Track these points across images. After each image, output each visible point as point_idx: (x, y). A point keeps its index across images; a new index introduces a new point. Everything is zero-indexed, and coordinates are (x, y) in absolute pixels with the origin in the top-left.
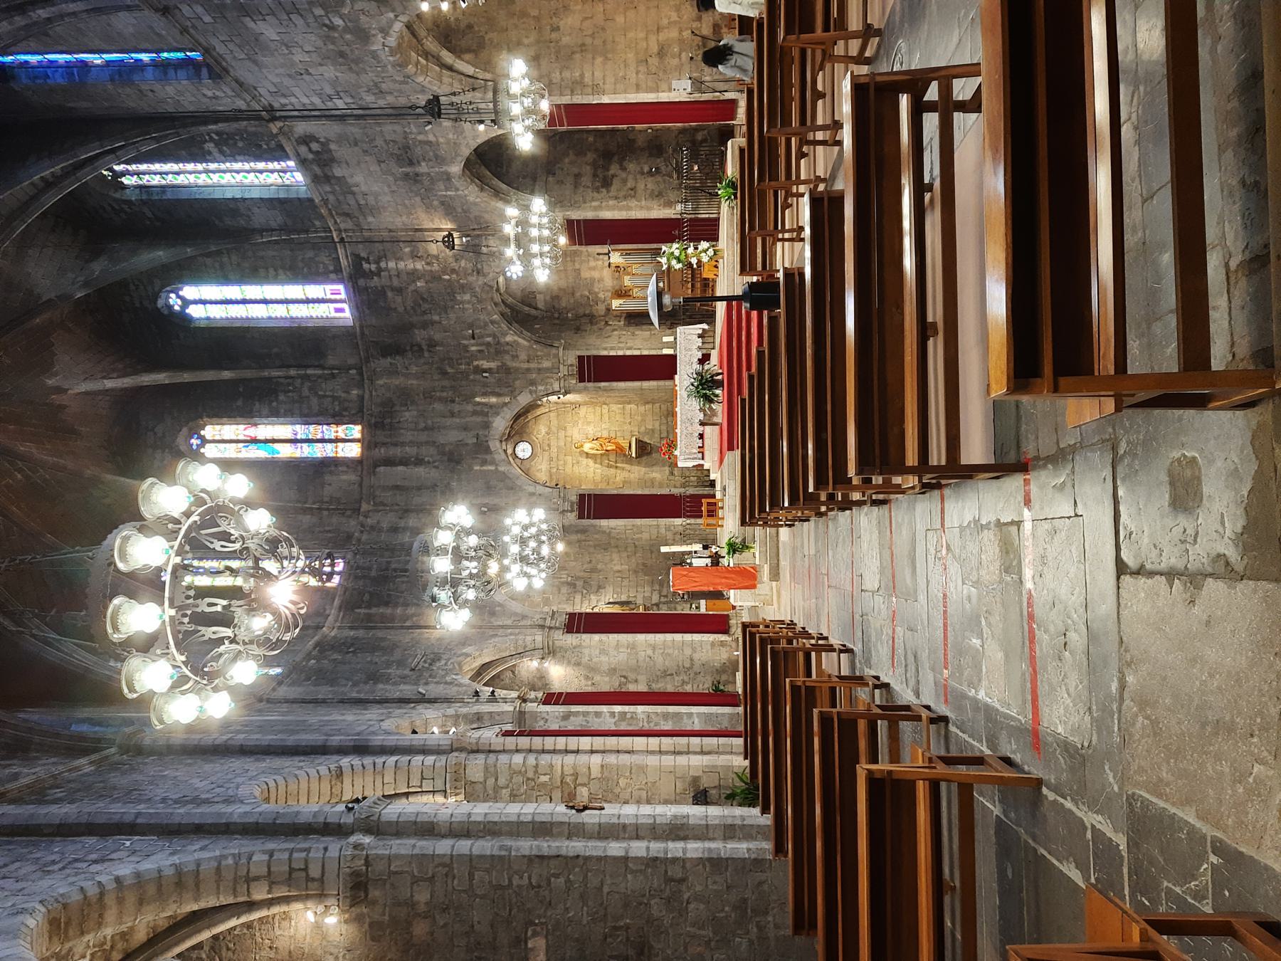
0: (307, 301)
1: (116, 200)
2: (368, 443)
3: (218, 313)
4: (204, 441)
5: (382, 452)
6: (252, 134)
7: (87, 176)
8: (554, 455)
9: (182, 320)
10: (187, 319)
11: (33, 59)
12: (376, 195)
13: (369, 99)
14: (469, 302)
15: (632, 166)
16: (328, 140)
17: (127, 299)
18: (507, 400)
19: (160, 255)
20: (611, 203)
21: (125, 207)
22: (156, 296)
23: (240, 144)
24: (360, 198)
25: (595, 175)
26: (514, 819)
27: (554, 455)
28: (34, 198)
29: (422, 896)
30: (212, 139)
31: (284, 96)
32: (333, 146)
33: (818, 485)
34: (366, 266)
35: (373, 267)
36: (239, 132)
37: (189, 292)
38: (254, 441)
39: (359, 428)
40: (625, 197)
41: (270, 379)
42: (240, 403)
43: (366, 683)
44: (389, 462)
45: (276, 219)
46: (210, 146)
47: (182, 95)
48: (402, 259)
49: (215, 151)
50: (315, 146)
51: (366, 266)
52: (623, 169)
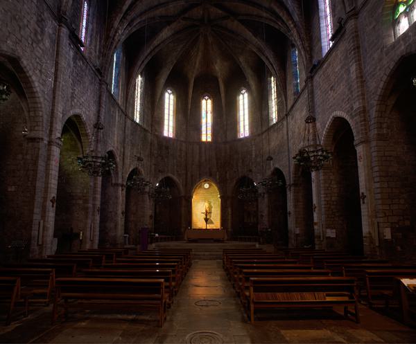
0: (244, 126)
3: (241, 102)
4: (206, 100)
6: (284, 113)
9: (238, 93)
10: (239, 95)
13: (292, 141)
19: (253, 87)
26: (50, 182)
29: (28, 157)
33: (255, 282)
37: (246, 95)
38: (207, 113)
39: (209, 139)
47: (290, 92)
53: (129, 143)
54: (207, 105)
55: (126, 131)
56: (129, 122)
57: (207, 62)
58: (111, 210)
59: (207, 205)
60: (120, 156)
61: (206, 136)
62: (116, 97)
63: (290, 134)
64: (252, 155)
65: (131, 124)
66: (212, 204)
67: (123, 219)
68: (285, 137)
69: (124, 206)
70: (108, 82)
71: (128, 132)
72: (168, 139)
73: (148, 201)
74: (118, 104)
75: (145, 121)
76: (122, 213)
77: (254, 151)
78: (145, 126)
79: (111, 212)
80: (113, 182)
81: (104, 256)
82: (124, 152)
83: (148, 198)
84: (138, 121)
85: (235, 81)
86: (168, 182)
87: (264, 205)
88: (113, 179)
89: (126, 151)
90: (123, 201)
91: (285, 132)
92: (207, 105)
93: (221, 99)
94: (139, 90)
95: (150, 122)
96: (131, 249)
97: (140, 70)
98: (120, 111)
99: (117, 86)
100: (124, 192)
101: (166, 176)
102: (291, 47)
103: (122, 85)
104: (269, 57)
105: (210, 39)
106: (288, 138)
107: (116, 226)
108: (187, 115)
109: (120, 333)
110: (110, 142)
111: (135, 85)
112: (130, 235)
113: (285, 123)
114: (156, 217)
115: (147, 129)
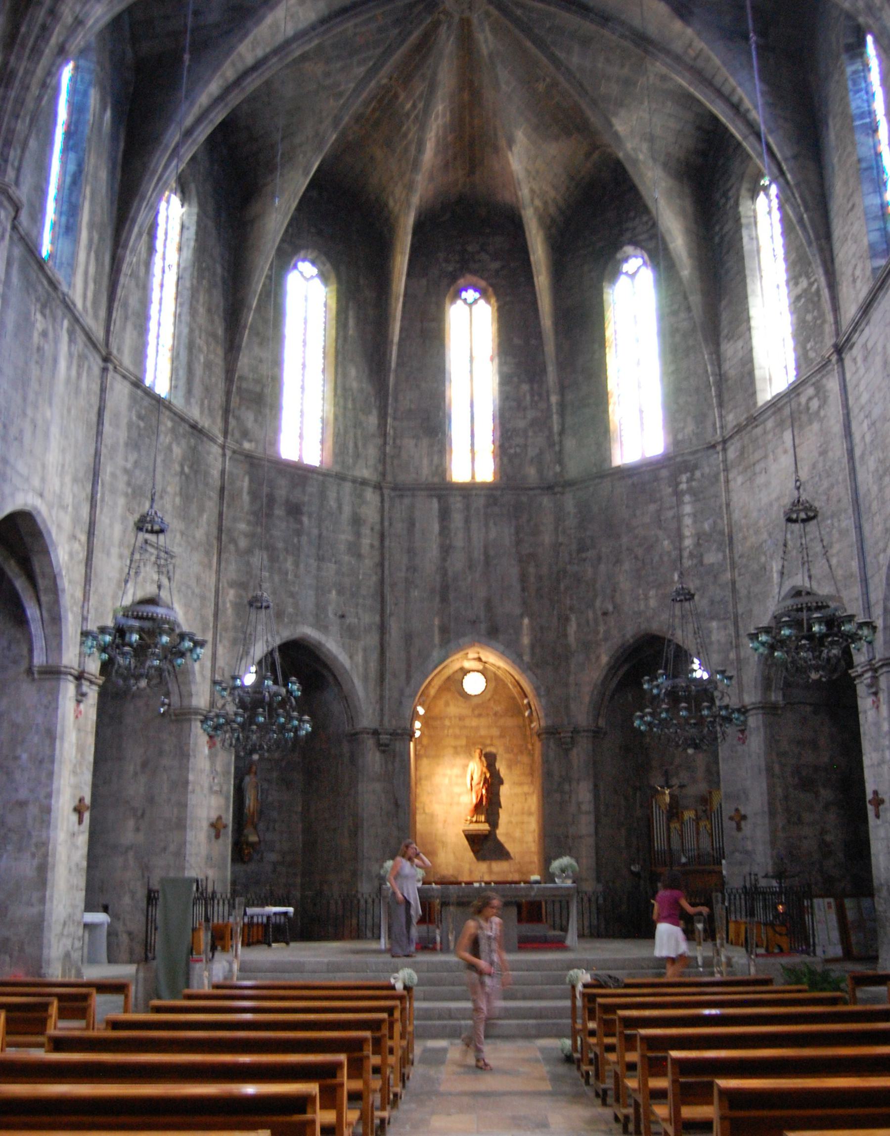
1: (738, 190)
2: (468, 490)
5: (457, 504)
7: (763, 163)
8: (467, 722)
9: (606, 265)
11: (875, 76)
12: (767, 484)
14: (647, 606)
15: (832, 817)
16: (821, 420)
17: (632, 214)
18: (526, 658)
20: (779, 791)
21: (732, 202)
22: (636, 243)
23: (809, 317)
24: (762, 465)
25: (816, 769)
27: (467, 722)
28: (719, 93)
30: (811, 284)
31: (865, 359)
32: (816, 426)
34: (684, 478)
35: (683, 486)
36: (822, 315)
40: (787, 810)
41: (544, 371)
42: (517, 341)
43: (129, 484)
44: (444, 515)
45: (731, 368)
46: (804, 283)
48: (695, 522)
49: (799, 290)
50: (814, 404)
51: (684, 478)
52: (826, 807)
53: (121, 485)
54: (471, 327)
55: (107, 428)
56: (120, 391)
57: (472, 144)
58: (23, 794)
59: (475, 768)
60: (74, 537)
61: (472, 456)
62: (60, 276)
63: (860, 429)
64: (680, 537)
65: (133, 399)
66: (502, 767)
67: (83, 840)
68: (838, 449)
69: (87, 777)
70: (23, 193)
71: (116, 433)
72: (299, 474)
73: (206, 751)
74: (68, 307)
75: (198, 390)
76: (78, 810)
77: (688, 521)
78: (195, 413)
79: (22, 804)
80: (39, 659)
81: (55, 1003)
82: (92, 525)
83: (203, 739)
84: (162, 389)
85: (599, 217)
86: (297, 660)
87: (746, 769)
88: (39, 643)
89: (104, 519)
90: (80, 748)
91: (837, 428)
92: (471, 327)
93: (534, 303)
94: (173, 257)
95: (219, 397)
96: (104, 988)
97: (180, 165)
98: (81, 338)
99: (68, 228)
100: (90, 708)
101: (287, 634)
102: (844, 57)
103: (91, 226)
104: (747, 95)
105: (486, 40)
106: (851, 452)
107: (43, 870)
108: (388, 366)
109: (714, 547)
110: (21, 466)
111: (152, 236)
112: (115, 916)
113: (832, 385)
114: (243, 834)
115: (205, 423)
